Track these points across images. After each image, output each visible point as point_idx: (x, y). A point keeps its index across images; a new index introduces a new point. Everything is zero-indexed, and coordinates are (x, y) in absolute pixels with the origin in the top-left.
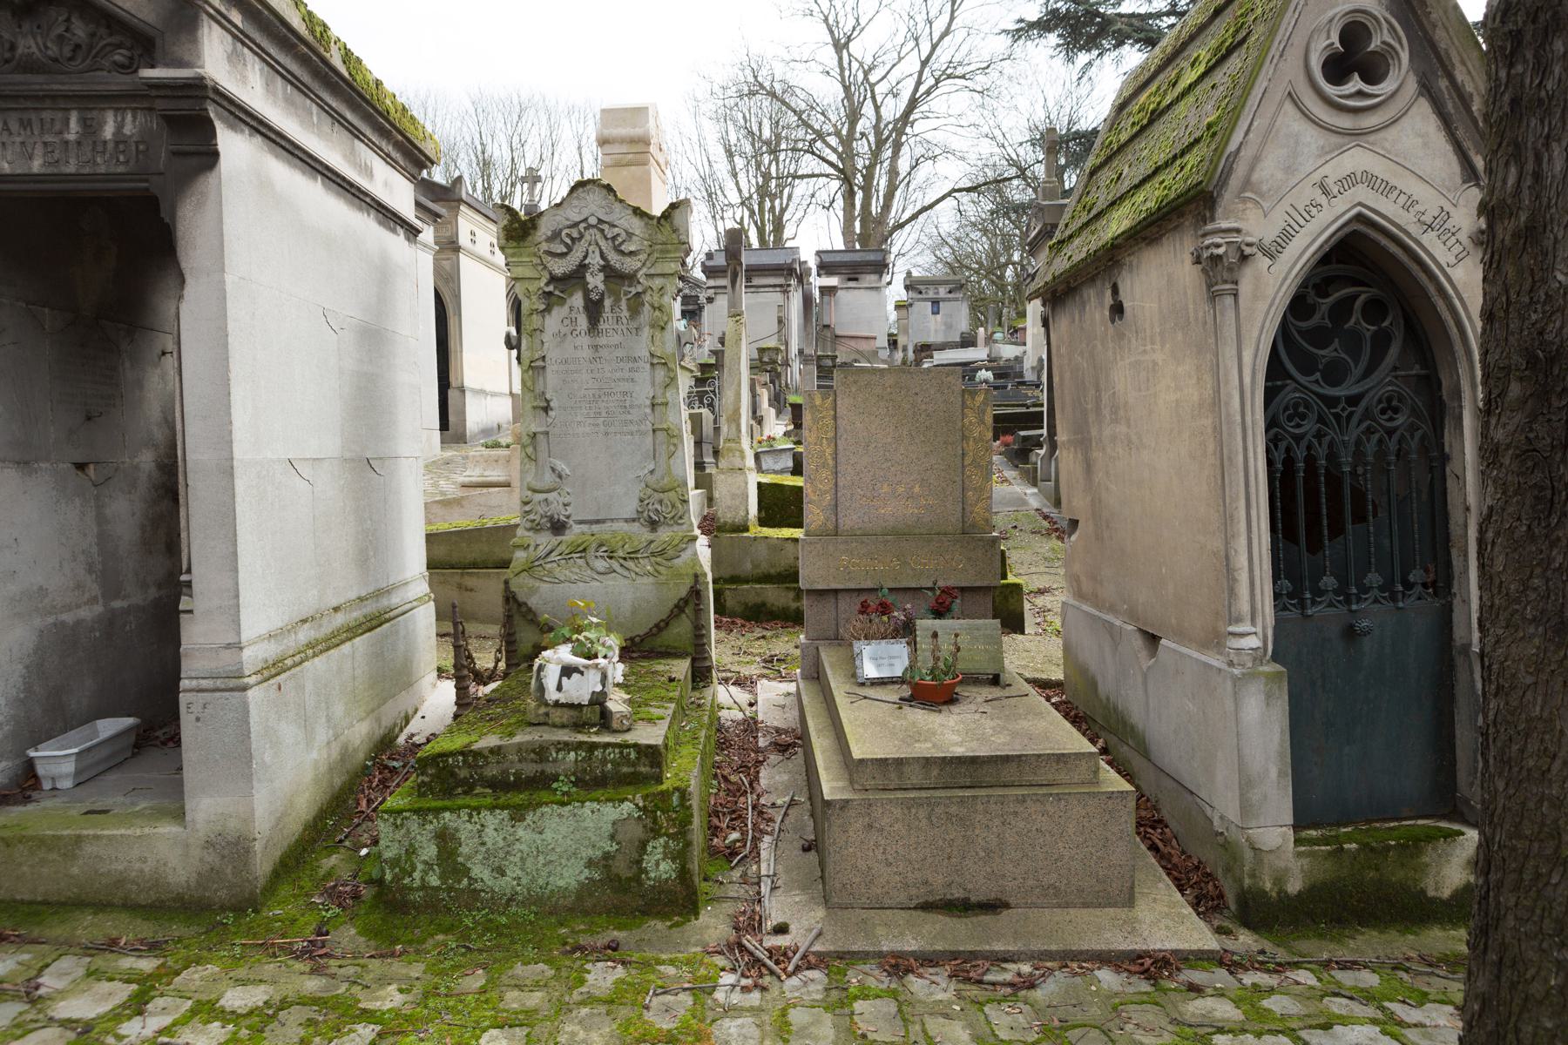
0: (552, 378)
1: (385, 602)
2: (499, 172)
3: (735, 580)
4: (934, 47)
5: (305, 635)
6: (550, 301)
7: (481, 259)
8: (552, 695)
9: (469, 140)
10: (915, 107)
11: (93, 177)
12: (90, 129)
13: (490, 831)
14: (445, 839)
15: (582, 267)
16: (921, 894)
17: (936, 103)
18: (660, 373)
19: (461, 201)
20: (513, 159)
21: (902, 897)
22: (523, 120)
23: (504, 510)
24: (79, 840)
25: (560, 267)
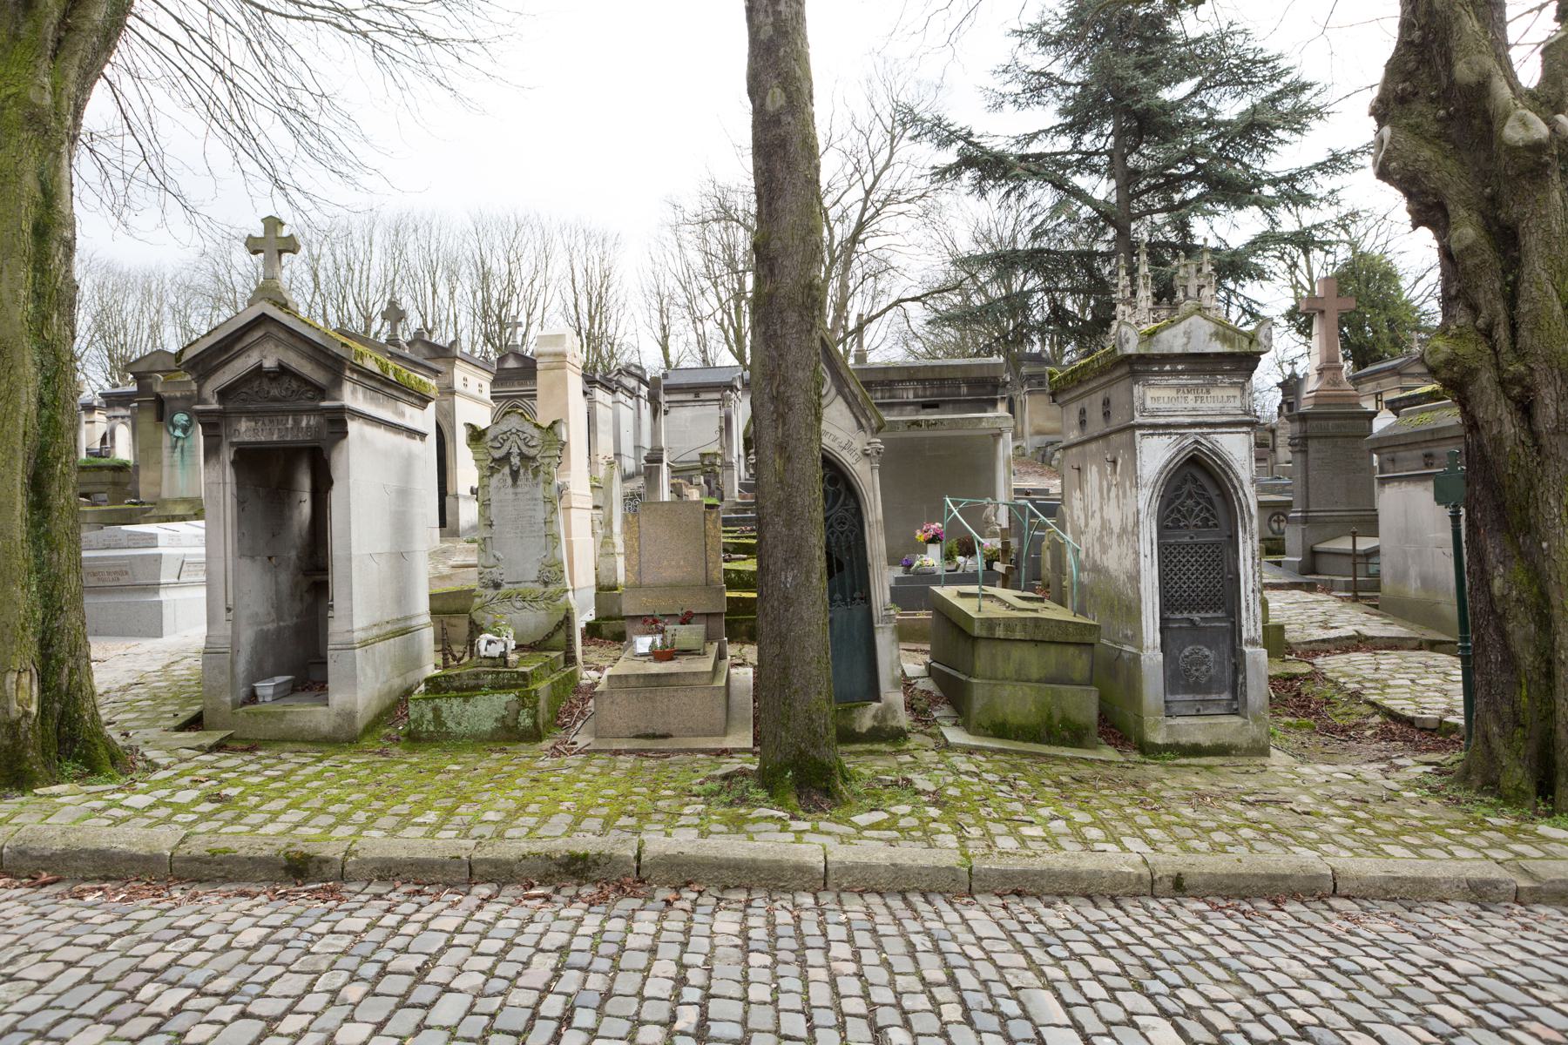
0: (494, 509)
1: (409, 623)
2: (498, 282)
3: (609, 618)
4: (877, 179)
5: (375, 631)
6: (493, 471)
7: (472, 398)
8: (483, 653)
9: (469, 253)
10: (863, 229)
11: (297, 442)
12: (297, 423)
13: (455, 707)
14: (436, 710)
15: (509, 454)
16: (635, 731)
17: (886, 223)
18: (549, 506)
19: (456, 357)
20: (510, 273)
21: (627, 733)
22: (520, 235)
23: (470, 580)
24: (284, 713)
25: (498, 454)
